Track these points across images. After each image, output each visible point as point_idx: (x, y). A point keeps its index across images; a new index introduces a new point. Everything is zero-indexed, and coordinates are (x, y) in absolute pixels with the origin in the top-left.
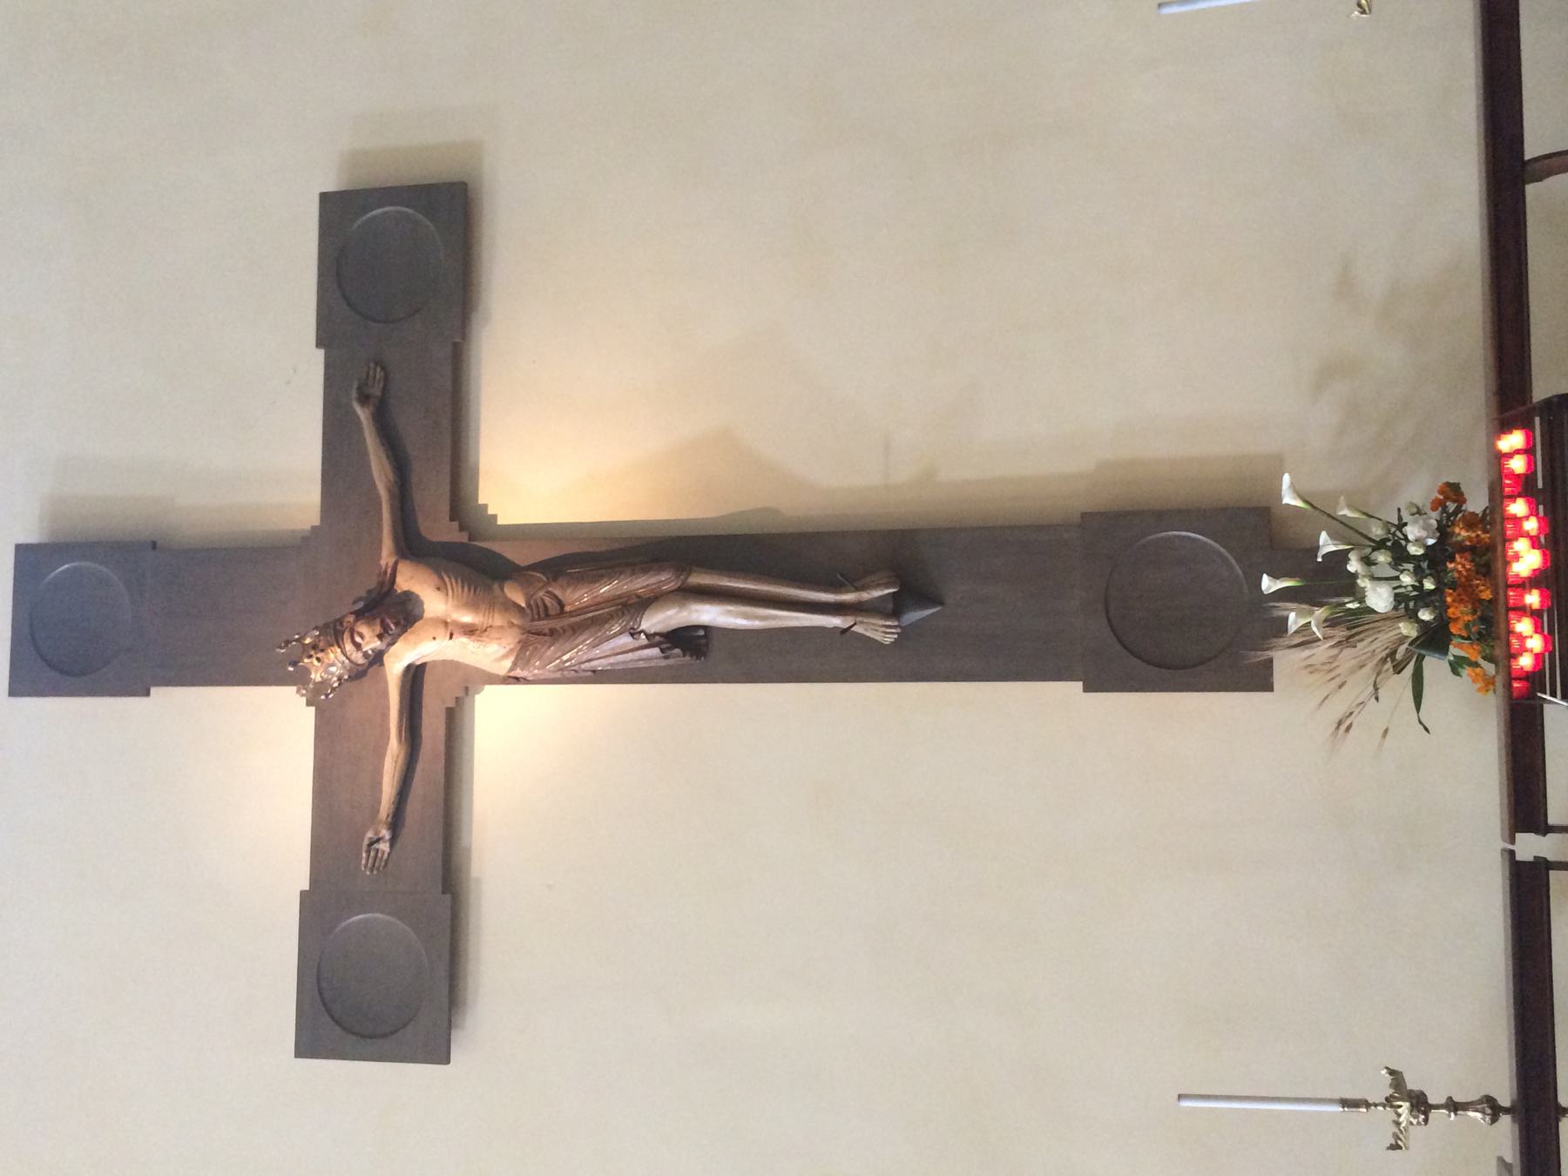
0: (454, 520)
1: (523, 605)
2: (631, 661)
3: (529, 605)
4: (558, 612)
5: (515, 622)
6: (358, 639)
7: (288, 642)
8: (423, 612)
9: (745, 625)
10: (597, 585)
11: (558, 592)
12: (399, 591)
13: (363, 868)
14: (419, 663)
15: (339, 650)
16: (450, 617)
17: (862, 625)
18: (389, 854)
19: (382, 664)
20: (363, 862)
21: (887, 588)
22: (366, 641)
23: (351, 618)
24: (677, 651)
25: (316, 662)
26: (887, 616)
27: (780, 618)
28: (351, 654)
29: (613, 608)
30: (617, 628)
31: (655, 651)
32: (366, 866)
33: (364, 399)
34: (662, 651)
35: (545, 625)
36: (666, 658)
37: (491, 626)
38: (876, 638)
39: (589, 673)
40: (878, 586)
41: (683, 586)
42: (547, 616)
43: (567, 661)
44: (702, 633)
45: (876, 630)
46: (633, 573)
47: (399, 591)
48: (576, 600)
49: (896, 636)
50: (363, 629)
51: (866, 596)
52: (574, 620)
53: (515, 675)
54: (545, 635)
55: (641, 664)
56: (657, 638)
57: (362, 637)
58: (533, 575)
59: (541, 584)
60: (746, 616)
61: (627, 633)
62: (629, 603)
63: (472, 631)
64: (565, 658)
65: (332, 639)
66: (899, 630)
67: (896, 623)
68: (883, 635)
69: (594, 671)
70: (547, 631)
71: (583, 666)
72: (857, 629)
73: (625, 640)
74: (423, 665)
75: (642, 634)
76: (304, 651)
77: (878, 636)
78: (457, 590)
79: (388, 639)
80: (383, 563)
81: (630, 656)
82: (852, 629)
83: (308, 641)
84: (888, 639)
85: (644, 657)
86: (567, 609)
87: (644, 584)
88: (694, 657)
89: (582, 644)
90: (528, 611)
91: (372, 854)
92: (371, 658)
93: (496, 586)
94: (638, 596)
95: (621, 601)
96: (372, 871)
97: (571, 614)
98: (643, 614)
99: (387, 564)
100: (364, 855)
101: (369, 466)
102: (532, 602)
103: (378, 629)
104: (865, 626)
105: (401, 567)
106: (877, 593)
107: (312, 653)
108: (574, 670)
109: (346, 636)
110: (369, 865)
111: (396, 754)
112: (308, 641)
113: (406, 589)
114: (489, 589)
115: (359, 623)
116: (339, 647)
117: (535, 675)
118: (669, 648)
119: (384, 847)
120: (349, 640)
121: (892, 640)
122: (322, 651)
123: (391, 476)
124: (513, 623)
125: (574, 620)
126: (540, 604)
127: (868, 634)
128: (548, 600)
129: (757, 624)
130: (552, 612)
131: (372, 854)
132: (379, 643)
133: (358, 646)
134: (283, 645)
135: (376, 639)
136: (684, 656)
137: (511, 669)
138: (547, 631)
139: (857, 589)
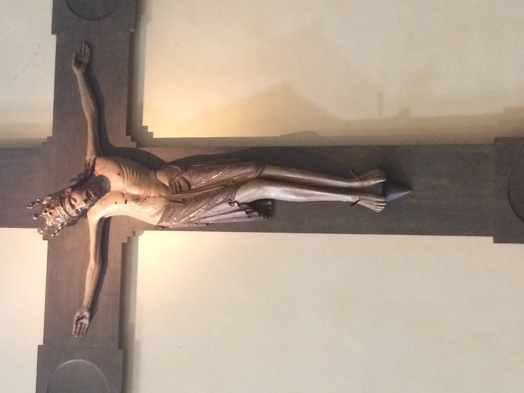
1: (168, 185)
2: (231, 218)
3: (171, 185)
5: (163, 194)
6: (73, 202)
7: (33, 203)
8: (110, 187)
10: (210, 174)
11: (187, 178)
13: (73, 333)
18: (88, 326)
20: (74, 330)
23: (69, 190)
24: (255, 213)
25: (49, 215)
26: (378, 195)
29: (218, 188)
31: (243, 213)
32: (75, 332)
33: (78, 64)
34: (247, 213)
36: (249, 217)
43: (192, 218)
44: (270, 203)
46: (231, 168)
48: (197, 183)
50: (76, 196)
51: (366, 184)
52: (197, 194)
54: (179, 202)
55: (235, 221)
56: (244, 206)
57: (75, 201)
60: (296, 194)
62: (228, 185)
63: (138, 199)
66: (385, 204)
67: (384, 200)
69: (207, 224)
71: (201, 221)
72: (361, 203)
73: (226, 206)
74: (110, 218)
77: (373, 207)
79: (90, 203)
80: (88, 159)
82: (358, 203)
84: (379, 209)
86: (193, 187)
90: (170, 188)
91: (79, 325)
92: (80, 214)
94: (233, 181)
95: (222, 184)
97: (195, 190)
99: (90, 160)
100: (74, 326)
103: (85, 197)
105: (97, 161)
106: (373, 182)
107: (47, 209)
108: (196, 223)
109: (67, 200)
110: (77, 332)
112: (45, 203)
114: (147, 174)
119: (86, 322)
121: (383, 208)
122: (53, 208)
123: (93, 109)
124: (161, 195)
125: (197, 194)
126: (177, 183)
127: (366, 206)
128: (182, 183)
129: (302, 199)
130: (184, 189)
131: (79, 325)
132: (85, 205)
133: (73, 206)
134: (31, 204)
135: (83, 202)
137: (160, 222)
139: (361, 180)
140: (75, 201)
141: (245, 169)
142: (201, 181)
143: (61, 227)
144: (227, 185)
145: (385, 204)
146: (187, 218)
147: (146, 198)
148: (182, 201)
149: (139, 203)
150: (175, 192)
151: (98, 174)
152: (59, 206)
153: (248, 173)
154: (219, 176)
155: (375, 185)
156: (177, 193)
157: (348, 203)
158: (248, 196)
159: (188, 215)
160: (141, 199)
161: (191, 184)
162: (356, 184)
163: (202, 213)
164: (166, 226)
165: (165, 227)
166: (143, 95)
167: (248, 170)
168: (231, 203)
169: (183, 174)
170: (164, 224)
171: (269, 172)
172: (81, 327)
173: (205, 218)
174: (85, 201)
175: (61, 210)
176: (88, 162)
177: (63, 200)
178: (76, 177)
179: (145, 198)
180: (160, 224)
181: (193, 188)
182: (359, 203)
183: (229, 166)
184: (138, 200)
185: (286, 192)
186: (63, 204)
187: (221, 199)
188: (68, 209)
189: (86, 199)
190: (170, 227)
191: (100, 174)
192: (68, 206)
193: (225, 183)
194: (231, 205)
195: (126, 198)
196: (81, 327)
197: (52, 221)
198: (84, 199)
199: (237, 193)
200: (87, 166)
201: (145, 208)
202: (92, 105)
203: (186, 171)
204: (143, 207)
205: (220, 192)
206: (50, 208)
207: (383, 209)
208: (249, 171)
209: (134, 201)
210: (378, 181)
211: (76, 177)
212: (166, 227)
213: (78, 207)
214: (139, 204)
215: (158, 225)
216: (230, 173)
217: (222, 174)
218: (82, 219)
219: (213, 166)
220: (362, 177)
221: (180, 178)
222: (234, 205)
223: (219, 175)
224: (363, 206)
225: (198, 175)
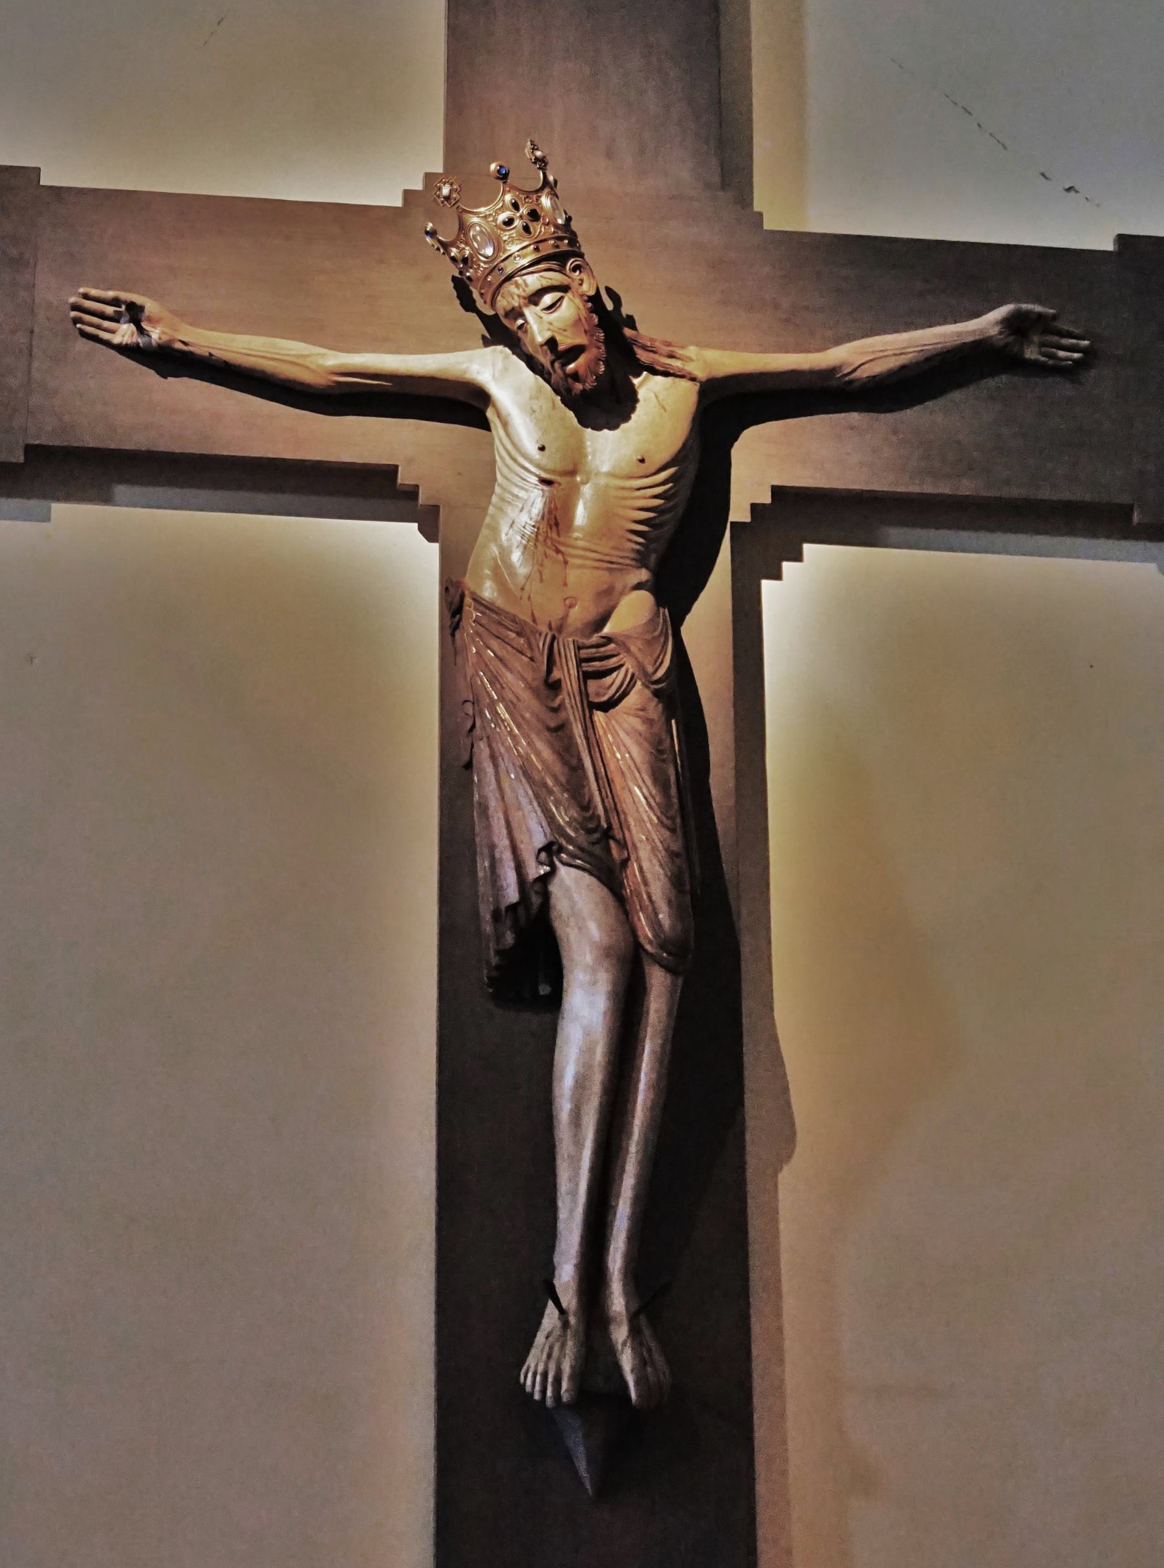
0: (26, 453)
1: (607, 630)
2: (492, 847)
3: (608, 640)
4: (595, 699)
5: (575, 612)
6: (548, 299)
7: (542, 163)
8: (598, 428)
9: (562, 1076)
10: (649, 782)
11: (633, 699)
12: (636, 381)
13: (81, 290)
14: (490, 414)
15: (525, 262)
16: (584, 483)
17: (559, 1324)
18: (108, 344)
19: (487, 343)
20: (94, 292)
21: (637, 1383)
22: (542, 314)
23: (588, 289)
24: (509, 938)
25: (503, 216)
26: (581, 1376)
27: (578, 1144)
28: (517, 285)
29: (600, 810)
30: (562, 819)
31: (512, 895)
32: (86, 296)
33: (1017, 325)
34: (512, 908)
35: (568, 673)
36: (496, 915)
37: (566, 562)
38: (531, 1361)
39: (466, 758)
40: (642, 1363)
41: (643, 955)
42: (587, 676)
43: (495, 713)
44: (544, 990)
45: (549, 1356)
46: (672, 855)
47: (636, 381)
48: (615, 734)
49: (537, 1397)
50: (570, 308)
51: (620, 1334)
52: (578, 730)
53: (466, 608)
54: (549, 671)
55: (483, 864)
56: (536, 900)
57: (551, 308)
58: (501, 561)
59: (650, 669)
60: (581, 1083)
61: (550, 838)
62: (612, 844)
63: (557, 524)
64: (501, 709)
65: (548, 248)
66: (549, 1402)
67: (565, 1397)
68: (541, 1368)
69: (469, 766)
70: (556, 674)
71: (482, 746)
72: (550, 1318)
73: (535, 835)
74: (485, 425)
75: (548, 868)
76: (528, 194)
77: (535, 1360)
78: (655, 497)
79: (545, 359)
80: (692, 351)
81: (503, 842)
82: (550, 1304)
83: (546, 201)
84: (530, 1380)
85: (500, 871)
86: (599, 716)
87: (649, 876)
88: (494, 974)
89: (528, 744)
90: (595, 639)
91: (110, 310)
92: (506, 322)
93: (644, 575)
94: (625, 863)
95: (615, 824)
96: (75, 307)
97: (589, 727)
98: (591, 873)
99: (691, 360)
100: (111, 294)
101: (945, 321)
102: (612, 646)
103: (564, 342)
104: (557, 1332)
105: (684, 384)
106: (627, 1361)
107: (524, 210)
108: (473, 726)
109: (555, 278)
110: (88, 304)
111: (307, 362)
112: (546, 201)
113: (640, 396)
114: (641, 560)
115: (578, 301)
116: (534, 263)
117: (466, 648)
118: (516, 921)
119: (125, 333)
120: (545, 283)
121: (528, 1389)
122: (526, 229)
123: (864, 373)
124: (571, 606)
125: (578, 730)
126: (613, 662)
127: (540, 1338)
128: (617, 678)
129: (564, 1108)
130: (592, 685)
131: (110, 310)
132: (540, 339)
133: (534, 298)
134: (538, 153)
135: (548, 335)
136: (498, 953)
137: (478, 601)
138: (556, 674)
139: (633, 1319)
140: (551, 308)
141: (669, 902)
142: (622, 748)
143: (459, 256)
144: (613, 838)
145: (549, 1402)
146: (621, 762)
147: (562, 553)
148: (551, 680)
149: (543, 527)
150: (584, 653)
151: (641, 384)
152: (537, 250)
153: (656, 915)
154: (641, 810)
155: (618, 1368)
156: (580, 661)
157: (549, 1269)
158: (575, 913)
159: (502, 699)
160: (559, 535)
161: (612, 711)
162: (617, 1302)
163: (508, 749)
164: (463, 623)
165: (458, 616)
166: (577, 508)
167: (664, 917)
168: (550, 850)
169: (645, 686)
170: (472, 612)
171: (658, 982)
172: (103, 316)
173: (493, 758)
174: (552, 343)
175: (524, 257)
176: (679, 352)
177: (553, 264)
178: (625, 311)
179: (562, 548)
180: (468, 600)
181: (596, 718)
182: (551, 1309)
183: (676, 846)
184: (552, 522)
185: (588, 1050)
186: (541, 266)
187: (564, 820)
188: (524, 281)
189: (559, 342)
190: (457, 636)
191: (642, 394)
192: (533, 281)
193: (617, 833)
194: (540, 851)
195: (560, 484)
196: (103, 316)
197: (480, 226)
198: (558, 338)
199: (587, 878)
200: (666, 349)
201: (525, 547)
202: (877, 368)
203: (657, 694)
204: (528, 541)
205: (588, 815)
206: (527, 220)
207: (532, 1394)
208: (661, 916)
209: (550, 512)
210: (630, 1379)
211: (625, 311)
212: (460, 620)
213: (530, 312)
214: (538, 529)
215: (466, 593)
216: (654, 849)
217: (651, 820)
218: (481, 329)
219: (674, 791)
220: (643, 1319)
221: (633, 676)
222: (541, 863)
223: (646, 812)
224: (538, 1324)
225: (646, 739)
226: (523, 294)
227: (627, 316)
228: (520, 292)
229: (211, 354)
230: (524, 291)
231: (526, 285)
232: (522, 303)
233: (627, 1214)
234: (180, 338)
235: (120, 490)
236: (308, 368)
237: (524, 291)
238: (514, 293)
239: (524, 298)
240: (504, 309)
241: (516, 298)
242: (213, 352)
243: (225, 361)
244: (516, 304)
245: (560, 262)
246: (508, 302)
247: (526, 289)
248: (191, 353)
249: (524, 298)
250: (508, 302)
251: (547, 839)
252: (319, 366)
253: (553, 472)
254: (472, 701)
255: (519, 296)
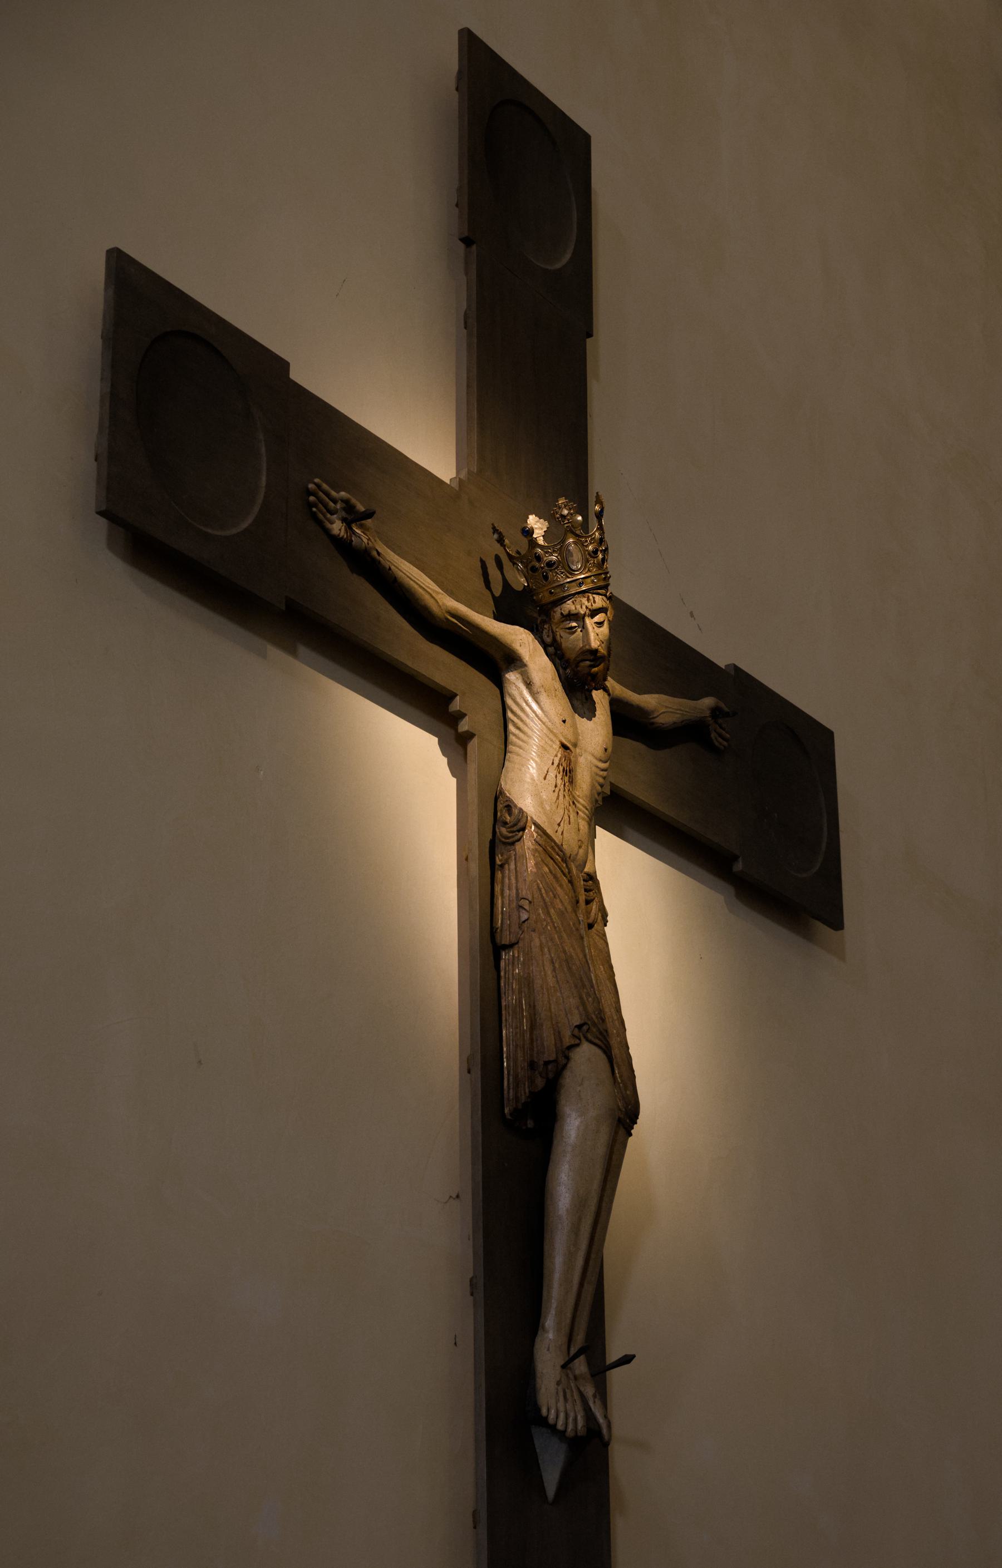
133: (594, 613)
188: (594, 598)
226: (590, 607)
227: (726, 666)
228: (589, 605)
229: (390, 569)
230: (592, 605)
231: (595, 602)
232: (587, 614)
233: (554, 1289)
234: (377, 548)
235: (302, 649)
236: (437, 602)
237: (592, 605)
238: (584, 604)
239: (590, 610)
240: (569, 611)
241: (584, 607)
242: (393, 567)
243: (395, 577)
244: (583, 612)
245: (517, 578)
246: (576, 609)
247: (593, 604)
248: (379, 562)
249: (590, 610)
250: (576, 609)
251: (581, 1020)
252: (444, 604)
253: (569, 741)
254: (530, 900)
255: (587, 607)
